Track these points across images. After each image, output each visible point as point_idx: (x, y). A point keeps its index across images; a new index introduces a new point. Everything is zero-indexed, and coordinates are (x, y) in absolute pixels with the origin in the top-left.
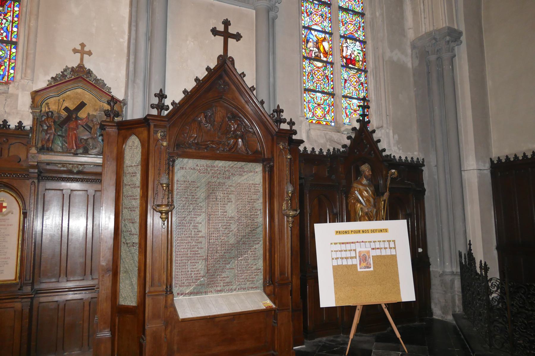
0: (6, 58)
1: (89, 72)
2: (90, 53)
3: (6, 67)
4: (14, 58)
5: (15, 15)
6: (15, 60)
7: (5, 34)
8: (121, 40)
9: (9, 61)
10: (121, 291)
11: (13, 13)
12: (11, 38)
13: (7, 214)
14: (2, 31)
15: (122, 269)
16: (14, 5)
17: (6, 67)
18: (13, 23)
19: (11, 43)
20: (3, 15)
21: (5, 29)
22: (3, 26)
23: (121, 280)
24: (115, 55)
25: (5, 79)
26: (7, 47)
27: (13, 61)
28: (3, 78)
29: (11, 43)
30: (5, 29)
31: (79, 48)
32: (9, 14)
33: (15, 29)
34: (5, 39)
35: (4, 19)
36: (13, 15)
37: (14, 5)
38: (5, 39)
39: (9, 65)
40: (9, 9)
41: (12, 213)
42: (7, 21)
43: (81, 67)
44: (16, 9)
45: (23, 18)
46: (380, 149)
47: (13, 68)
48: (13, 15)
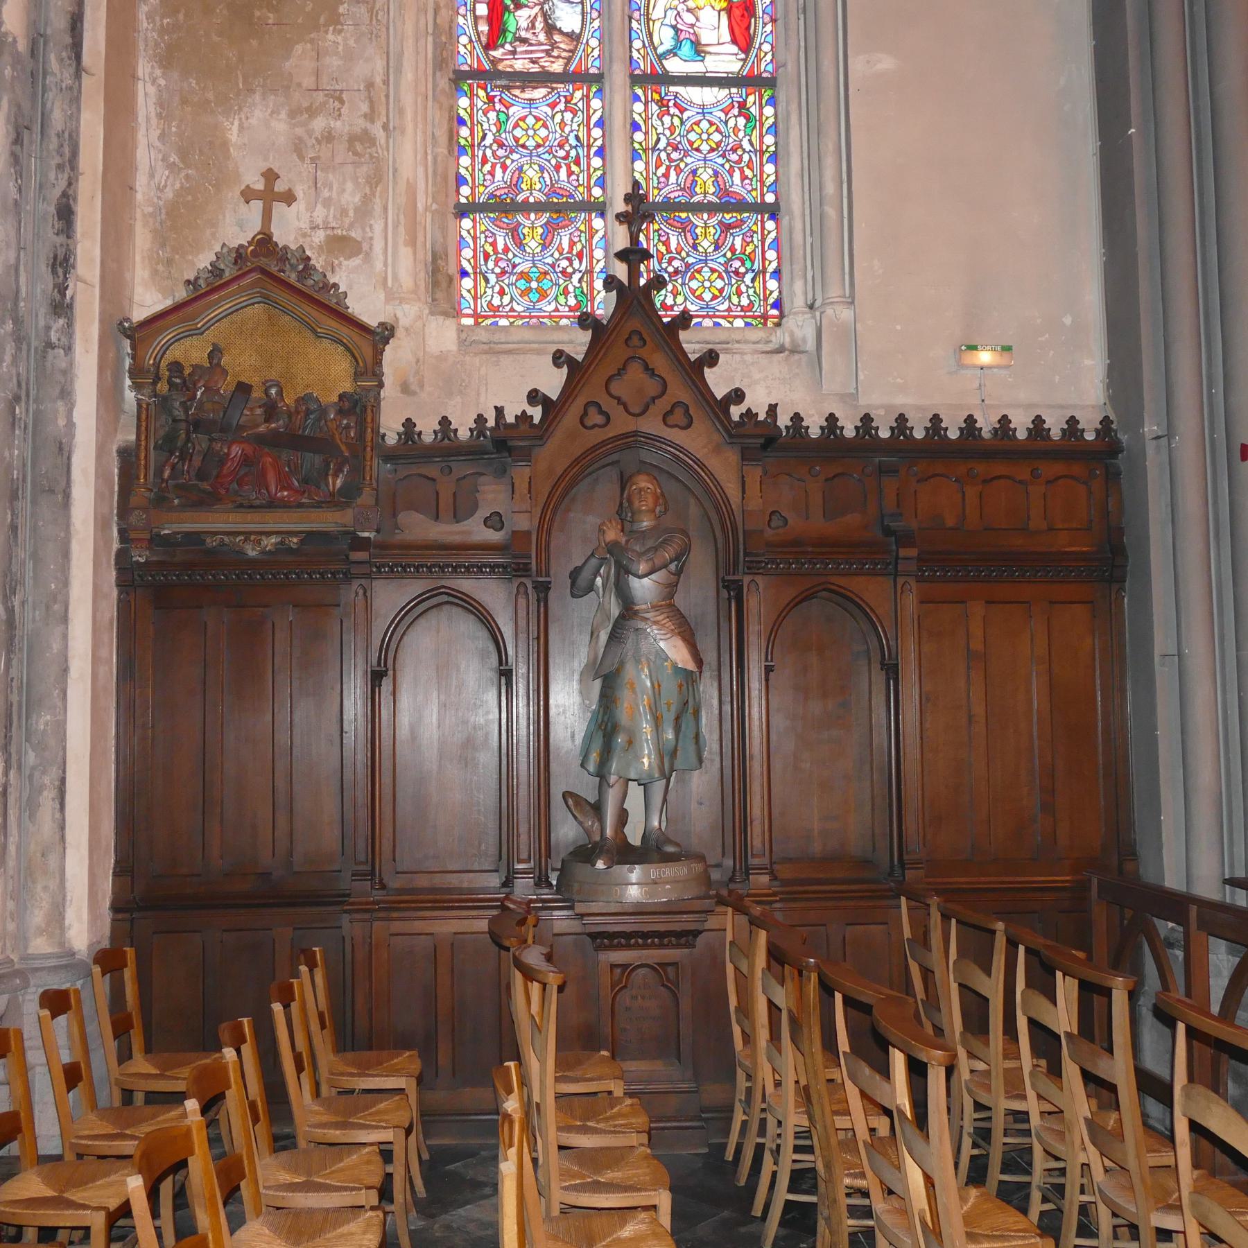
43: (264, 242)
46: (719, 395)
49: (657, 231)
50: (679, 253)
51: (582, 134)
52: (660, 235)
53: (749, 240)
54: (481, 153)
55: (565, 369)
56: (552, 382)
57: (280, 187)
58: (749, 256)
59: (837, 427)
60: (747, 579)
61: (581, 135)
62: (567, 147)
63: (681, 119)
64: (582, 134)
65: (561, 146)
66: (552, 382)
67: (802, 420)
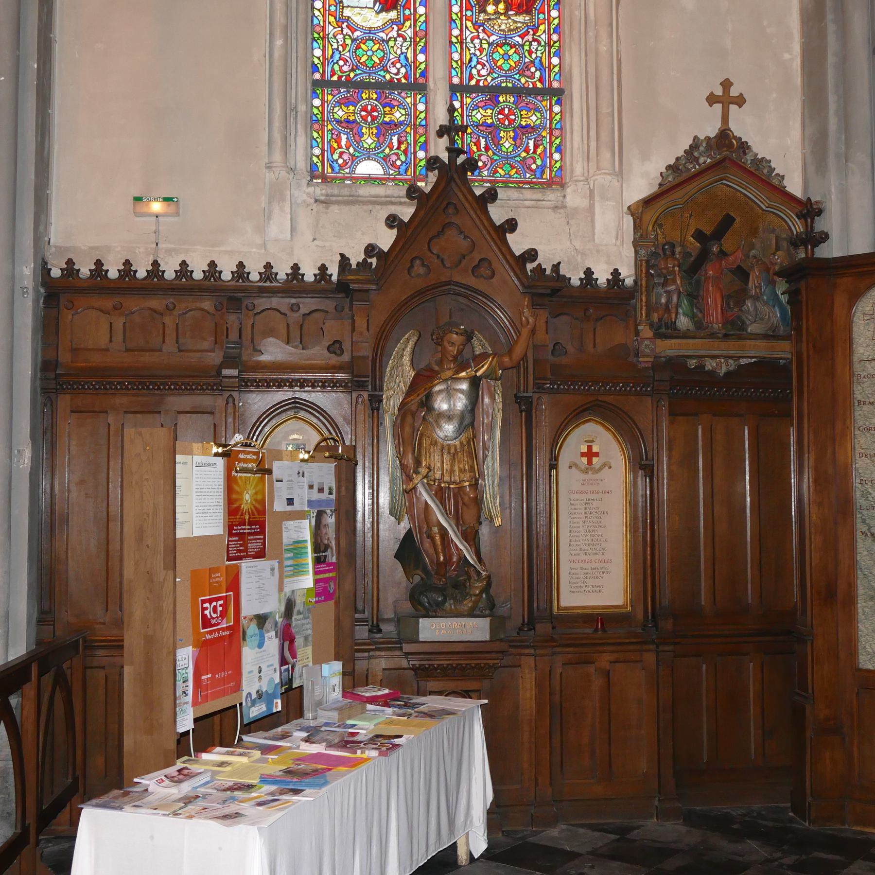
0: (544, 128)
1: (744, 147)
2: (740, 101)
3: (545, 148)
4: (559, 126)
5: (553, 27)
6: (561, 129)
7: (538, 74)
8: (787, 56)
9: (551, 134)
10: (862, 639)
11: (415, 21)
12: (550, 82)
13: (601, 469)
14: (533, 70)
15: (861, 591)
16: (549, 6)
17: (545, 148)
18: (550, 47)
19: (550, 92)
20: (531, 32)
21: (537, 61)
22: (534, 56)
23: (861, 616)
24: (774, 95)
25: (547, 175)
26: (544, 103)
27: (557, 133)
28: (543, 172)
29: (550, 92)
30: (537, 61)
31: (734, 92)
32: (408, 24)
33: (555, 61)
34: (539, 85)
35: (534, 40)
36: (549, 29)
37: (549, 6)
38: (539, 85)
39: (551, 143)
40: (541, 16)
41: (610, 467)
42: (539, 43)
43: (724, 135)
44: (554, 13)
45: (566, 28)
47: (559, 149)
48: (549, 29)
49: (331, 130)
50: (348, 149)
51: (410, 55)
52: (332, 134)
53: (403, 139)
54: (330, 67)
55: (395, 231)
56: (386, 239)
57: (719, 92)
58: (539, 155)
59: (216, 271)
60: (536, 396)
61: (409, 55)
62: (398, 65)
63: (488, 43)
64: (410, 55)
65: (394, 64)
66: (386, 239)
67: (74, 264)
